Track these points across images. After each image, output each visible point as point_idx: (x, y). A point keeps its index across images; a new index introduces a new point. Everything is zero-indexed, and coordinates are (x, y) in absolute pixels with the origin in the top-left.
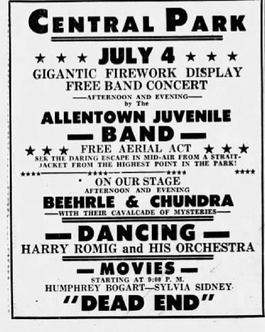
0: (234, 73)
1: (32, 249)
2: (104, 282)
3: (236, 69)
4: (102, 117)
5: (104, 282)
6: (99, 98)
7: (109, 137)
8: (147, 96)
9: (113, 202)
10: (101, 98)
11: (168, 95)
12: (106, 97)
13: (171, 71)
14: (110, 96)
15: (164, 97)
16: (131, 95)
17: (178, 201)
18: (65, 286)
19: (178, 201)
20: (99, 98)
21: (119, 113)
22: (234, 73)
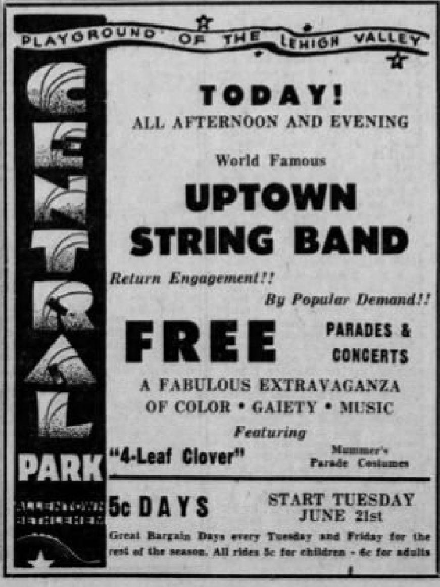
0: (403, 500)
1: (307, 385)
2: (298, 503)
3: (406, 495)
4: (258, 196)
5: (298, 503)
6: (200, 126)
7: (307, 245)
8: (314, 118)
9: (270, 341)
10: (205, 123)
11: (362, 116)
12: (217, 122)
14: (227, 118)
15: (352, 122)
16: (276, 116)
17: (198, 198)
18: (351, 404)
19: (198, 198)
20: (200, 126)
21: (296, 188)
22: (403, 500)
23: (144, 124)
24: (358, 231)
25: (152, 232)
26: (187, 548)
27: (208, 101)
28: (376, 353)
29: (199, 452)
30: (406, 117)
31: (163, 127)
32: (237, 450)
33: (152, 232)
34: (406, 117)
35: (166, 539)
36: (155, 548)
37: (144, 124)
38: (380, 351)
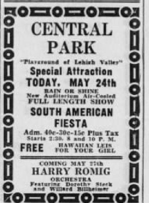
13: (89, 44)
23: (101, 31)
24: (74, 109)
25: (85, 93)
26: (51, 60)
27: (65, 63)
28: (35, 146)
29: (102, 70)
30: (109, 169)
31: (111, 34)
32: (120, 61)
33: (85, 93)
34: (109, 169)
35: (85, 70)
36: (112, 80)
37: (101, 31)
38: (38, 145)
